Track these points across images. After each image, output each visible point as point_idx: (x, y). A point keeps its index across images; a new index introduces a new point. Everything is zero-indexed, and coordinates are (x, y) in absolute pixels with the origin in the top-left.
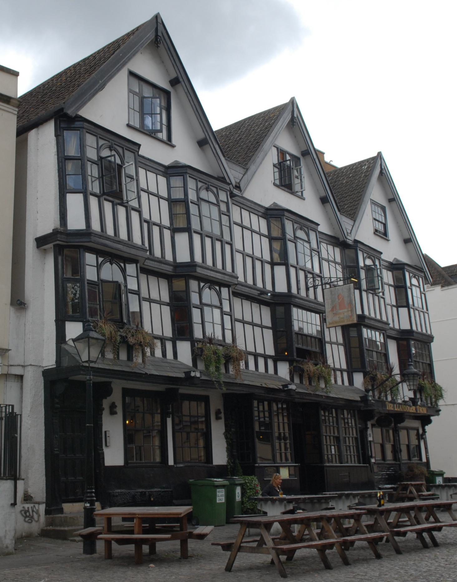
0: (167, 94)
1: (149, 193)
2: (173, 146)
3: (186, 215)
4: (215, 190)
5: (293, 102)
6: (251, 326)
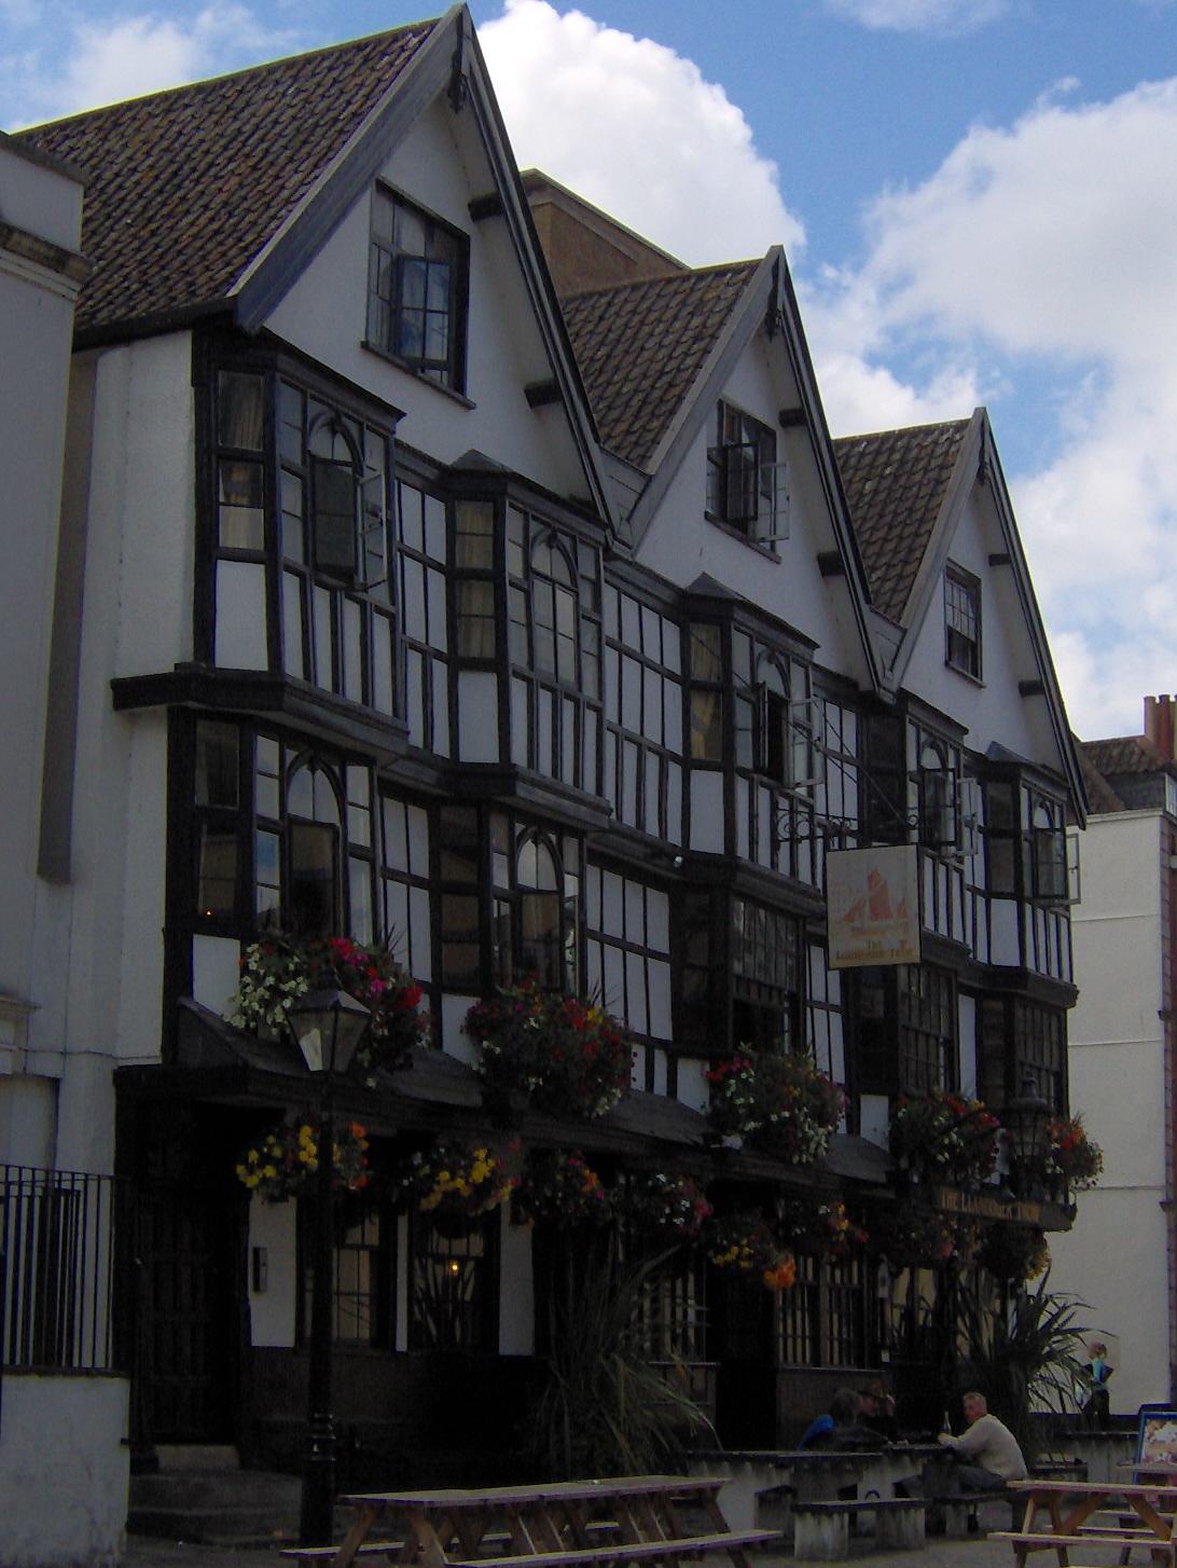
2: (468, 406)
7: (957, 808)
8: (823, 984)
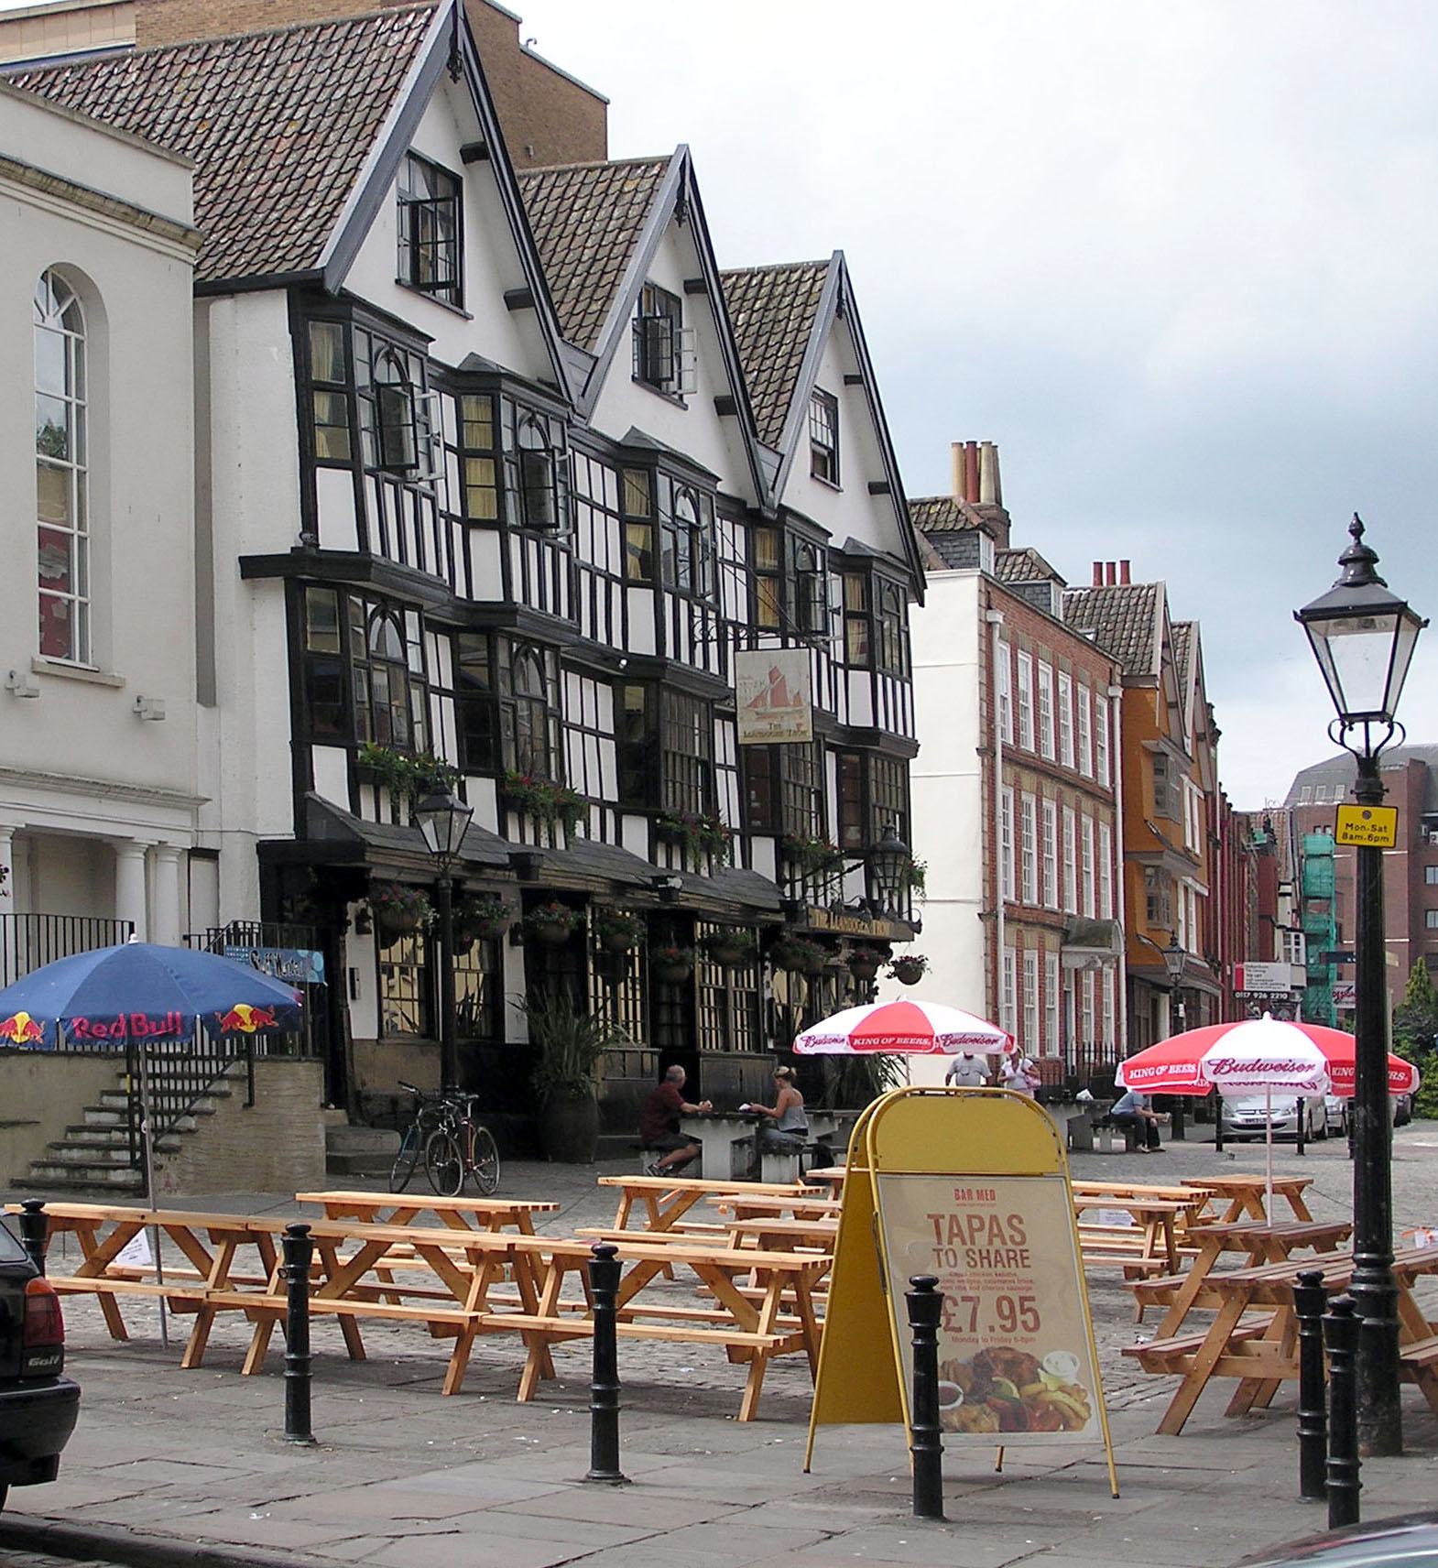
2: (467, 317)
3: (495, 491)
7: (824, 600)
8: (724, 750)
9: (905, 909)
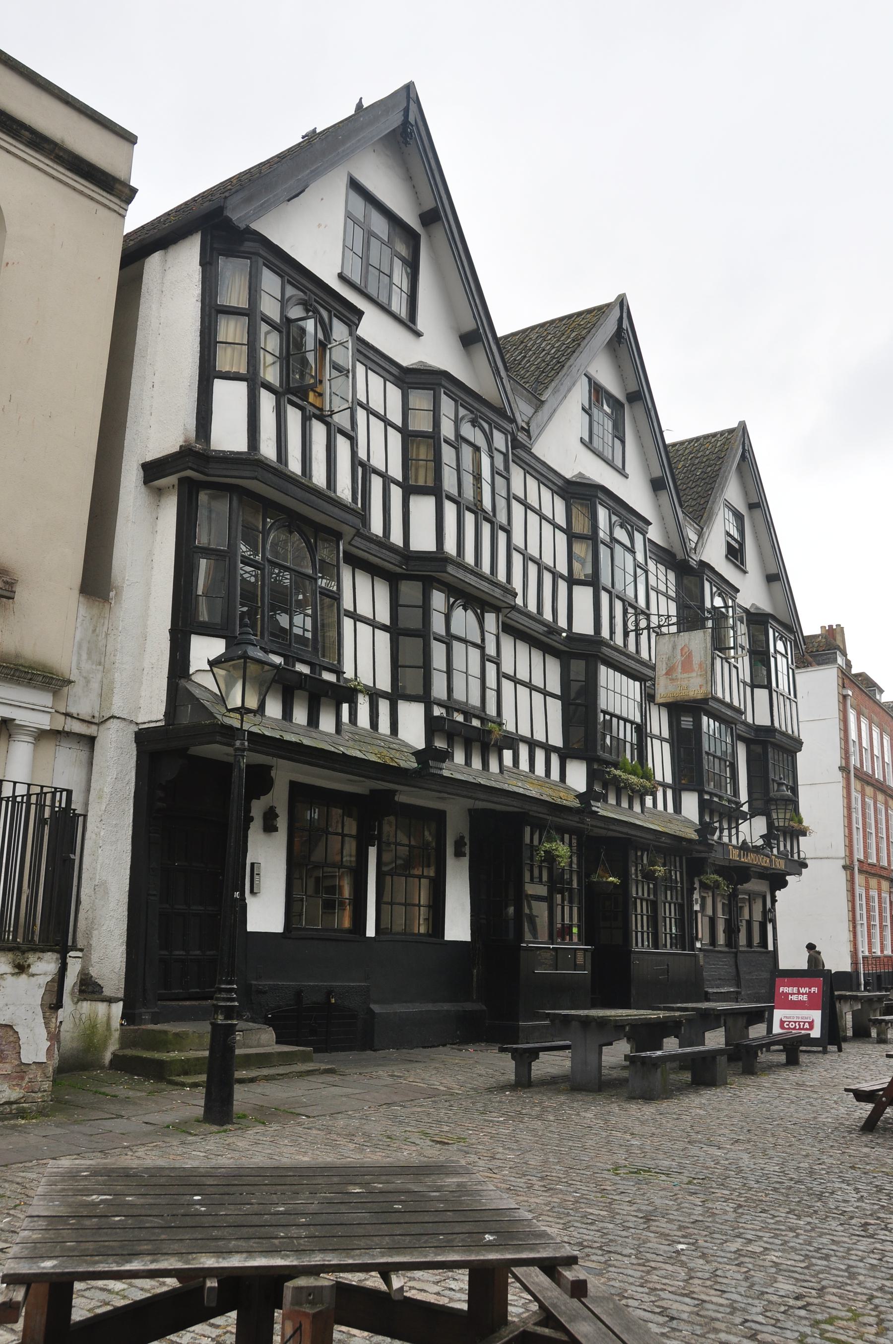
0: (412, 238)
1: (370, 412)
4: (486, 426)
5: (622, 302)
6: (528, 690)
9: (795, 850)
